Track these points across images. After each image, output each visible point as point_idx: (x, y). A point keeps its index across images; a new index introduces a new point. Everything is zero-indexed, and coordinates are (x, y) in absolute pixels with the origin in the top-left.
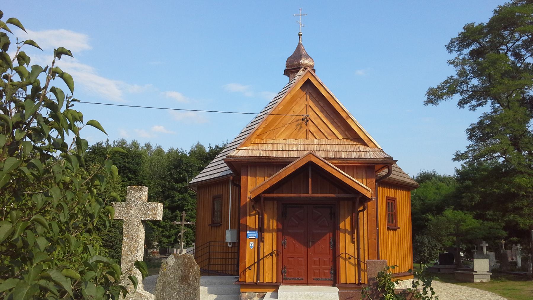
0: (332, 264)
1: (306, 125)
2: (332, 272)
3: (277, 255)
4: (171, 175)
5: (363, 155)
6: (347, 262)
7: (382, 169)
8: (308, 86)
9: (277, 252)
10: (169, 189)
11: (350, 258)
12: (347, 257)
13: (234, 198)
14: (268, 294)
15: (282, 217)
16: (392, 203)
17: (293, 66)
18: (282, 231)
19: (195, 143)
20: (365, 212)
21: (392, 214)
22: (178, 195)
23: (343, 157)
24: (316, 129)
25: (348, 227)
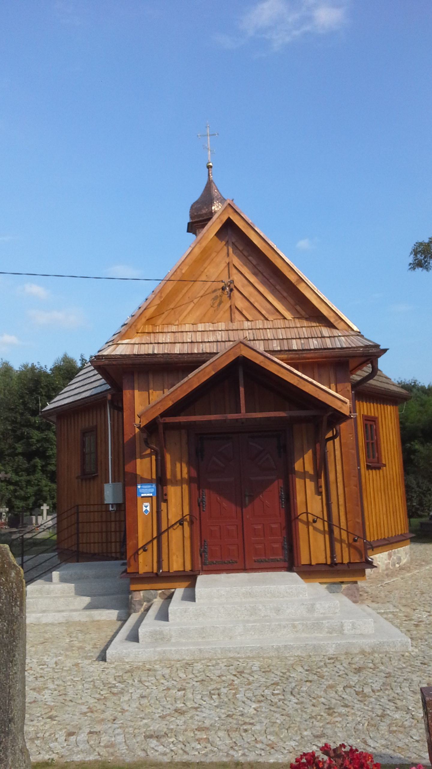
0: (284, 532)
1: (230, 297)
2: (286, 546)
3: (191, 523)
4: (24, 404)
5: (329, 343)
6: (311, 528)
7: (359, 366)
8: (230, 232)
9: (190, 518)
10: (23, 426)
11: (314, 521)
12: (311, 518)
13: (116, 430)
14: (179, 592)
15: (197, 458)
16: (371, 426)
17: (201, 216)
18: (198, 482)
19: (61, 356)
20: (337, 441)
21: (372, 443)
22: (36, 435)
23: (295, 347)
24: (247, 303)
25: (309, 468)
